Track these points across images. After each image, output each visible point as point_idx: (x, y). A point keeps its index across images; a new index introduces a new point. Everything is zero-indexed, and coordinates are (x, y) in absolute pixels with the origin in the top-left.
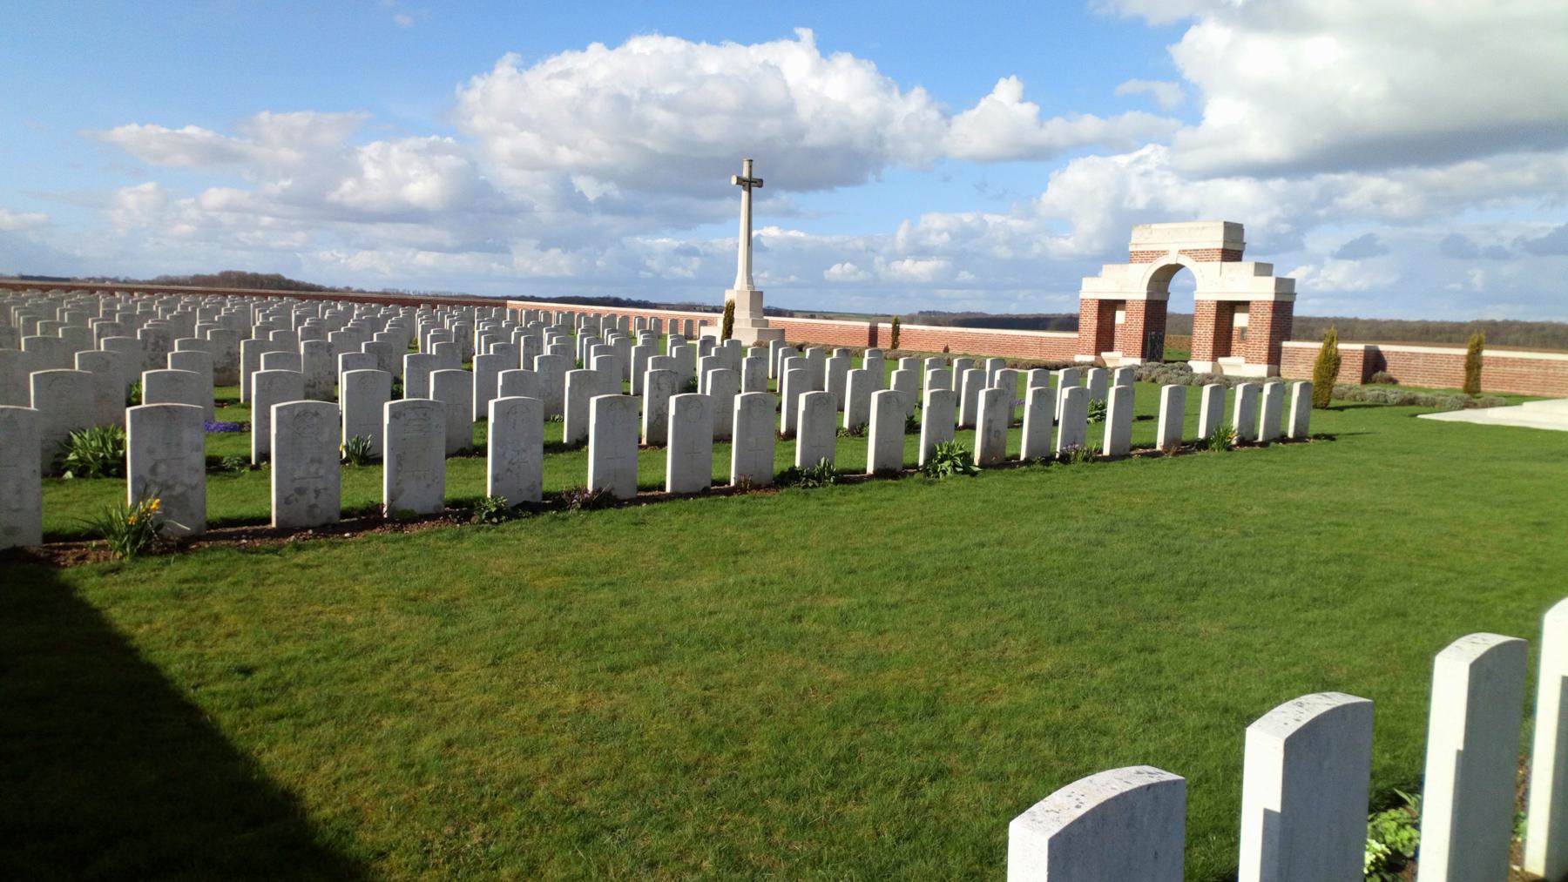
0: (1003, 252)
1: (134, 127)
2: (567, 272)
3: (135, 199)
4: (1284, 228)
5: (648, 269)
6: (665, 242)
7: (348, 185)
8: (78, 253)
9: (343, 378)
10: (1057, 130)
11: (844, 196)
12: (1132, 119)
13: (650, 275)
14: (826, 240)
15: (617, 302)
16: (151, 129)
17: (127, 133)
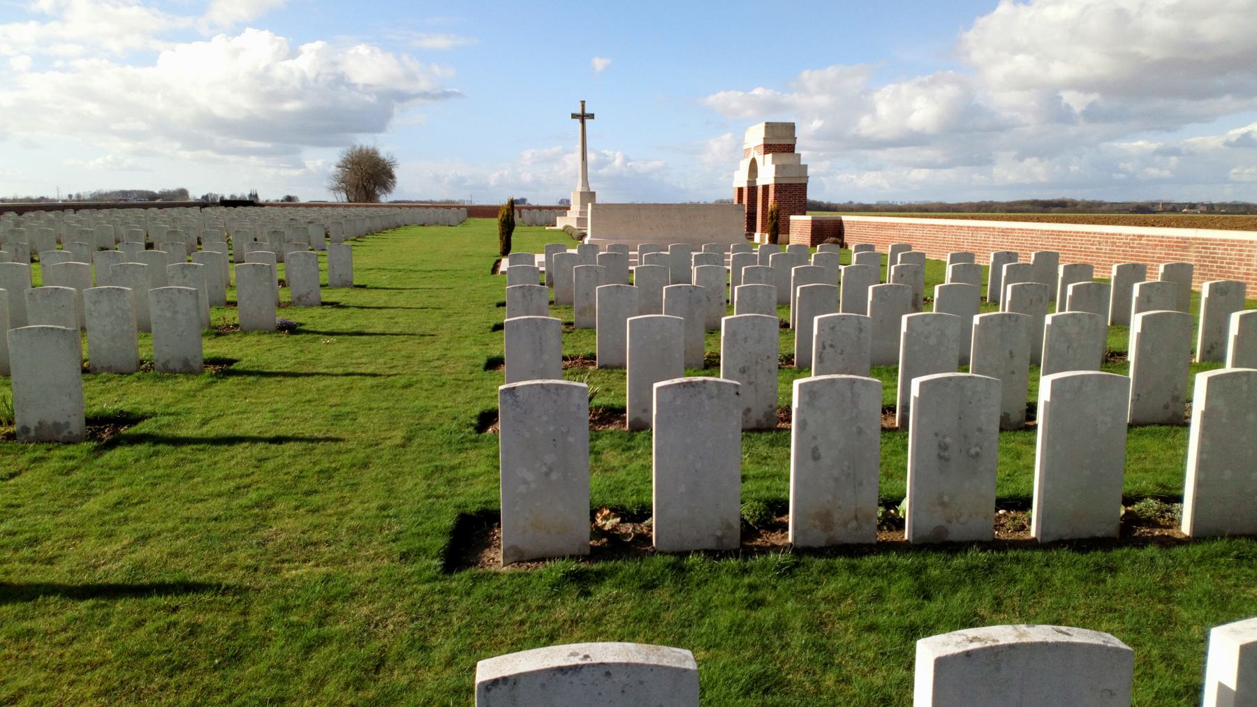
1: (722, 94)
2: (1043, 179)
6: (1141, 144)
8: (683, 186)
13: (1122, 176)
15: (1143, 213)
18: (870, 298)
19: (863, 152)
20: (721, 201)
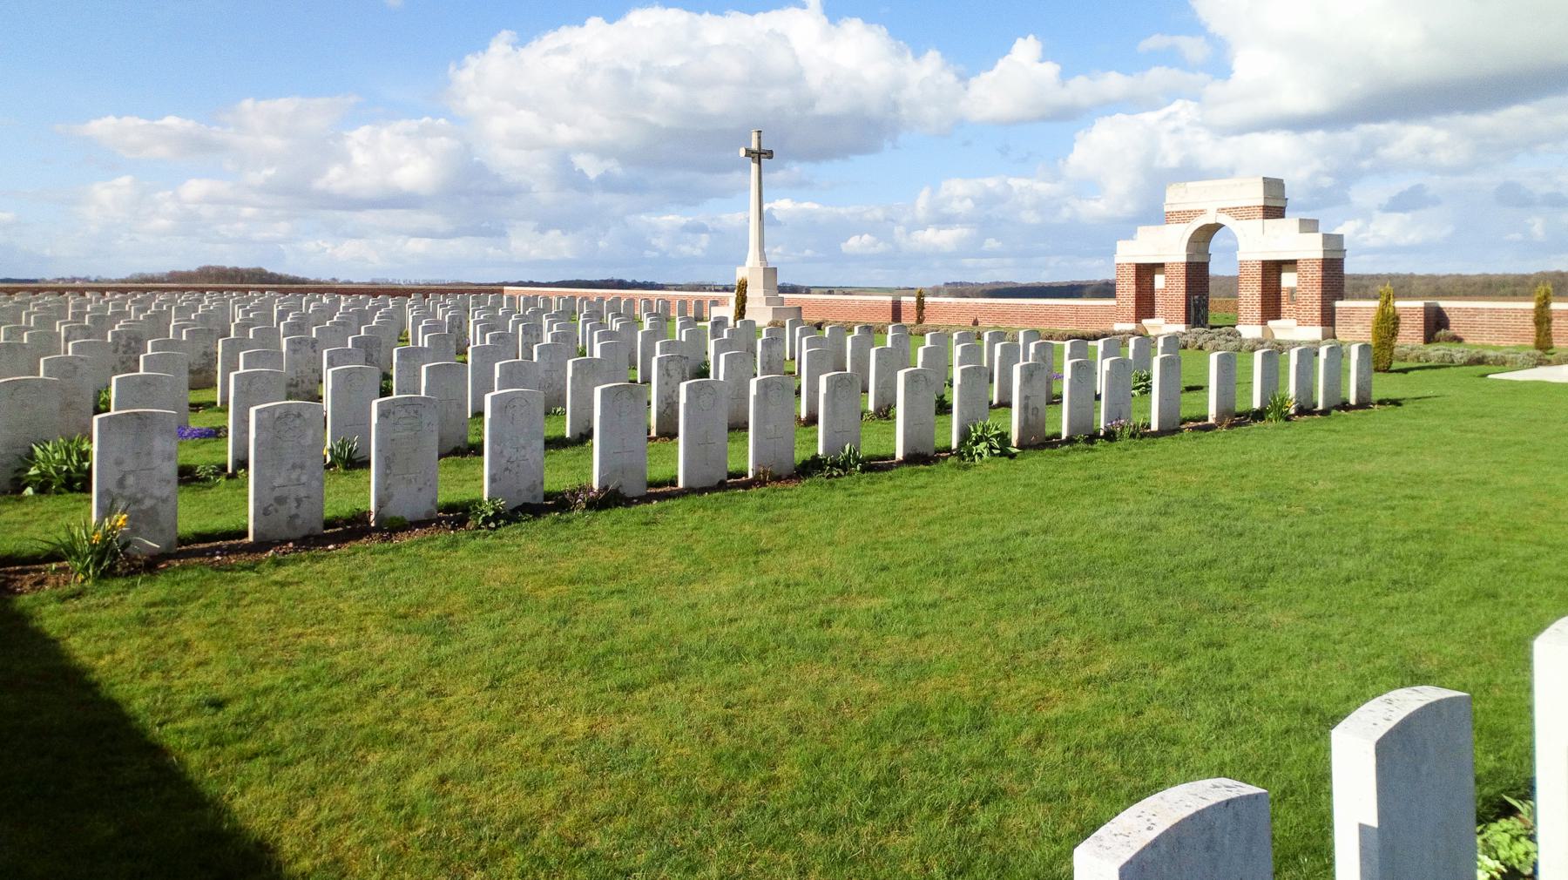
0: (1031, 218)
2: (568, 255)
3: (109, 195)
4: (1327, 182)
5: (654, 248)
6: (671, 219)
7: (335, 172)
8: (47, 252)
10: (1081, 89)
11: (859, 165)
12: (1159, 76)
13: (656, 254)
14: (842, 211)
16: (129, 121)
17: (103, 126)
18: (497, 375)
19: (338, 214)
20: (208, 268)
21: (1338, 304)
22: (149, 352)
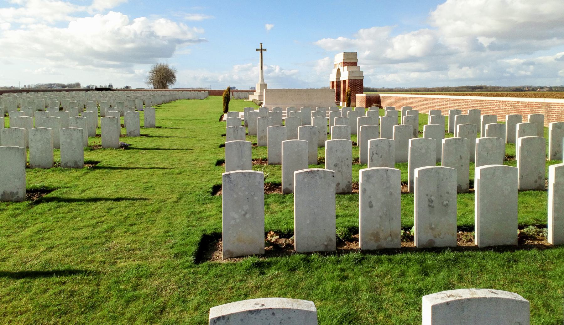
6: (516, 61)
9: (312, 118)
13: (508, 75)
17: (322, 42)
20: (324, 88)
21: (357, 95)
22: (429, 124)
